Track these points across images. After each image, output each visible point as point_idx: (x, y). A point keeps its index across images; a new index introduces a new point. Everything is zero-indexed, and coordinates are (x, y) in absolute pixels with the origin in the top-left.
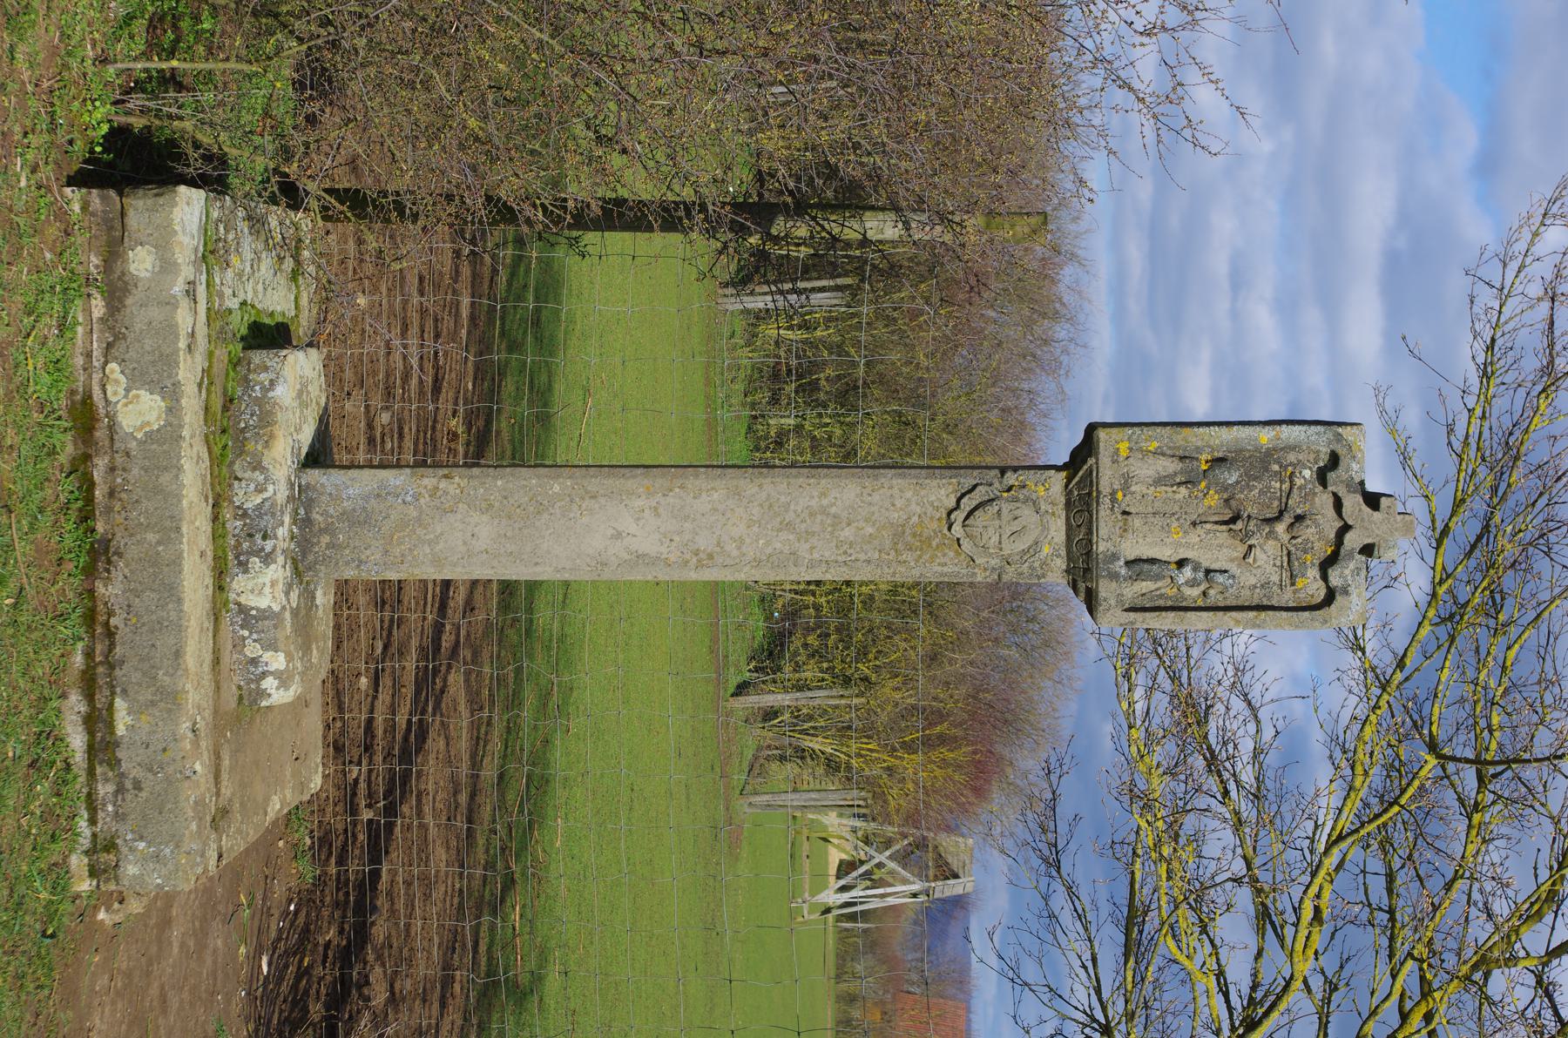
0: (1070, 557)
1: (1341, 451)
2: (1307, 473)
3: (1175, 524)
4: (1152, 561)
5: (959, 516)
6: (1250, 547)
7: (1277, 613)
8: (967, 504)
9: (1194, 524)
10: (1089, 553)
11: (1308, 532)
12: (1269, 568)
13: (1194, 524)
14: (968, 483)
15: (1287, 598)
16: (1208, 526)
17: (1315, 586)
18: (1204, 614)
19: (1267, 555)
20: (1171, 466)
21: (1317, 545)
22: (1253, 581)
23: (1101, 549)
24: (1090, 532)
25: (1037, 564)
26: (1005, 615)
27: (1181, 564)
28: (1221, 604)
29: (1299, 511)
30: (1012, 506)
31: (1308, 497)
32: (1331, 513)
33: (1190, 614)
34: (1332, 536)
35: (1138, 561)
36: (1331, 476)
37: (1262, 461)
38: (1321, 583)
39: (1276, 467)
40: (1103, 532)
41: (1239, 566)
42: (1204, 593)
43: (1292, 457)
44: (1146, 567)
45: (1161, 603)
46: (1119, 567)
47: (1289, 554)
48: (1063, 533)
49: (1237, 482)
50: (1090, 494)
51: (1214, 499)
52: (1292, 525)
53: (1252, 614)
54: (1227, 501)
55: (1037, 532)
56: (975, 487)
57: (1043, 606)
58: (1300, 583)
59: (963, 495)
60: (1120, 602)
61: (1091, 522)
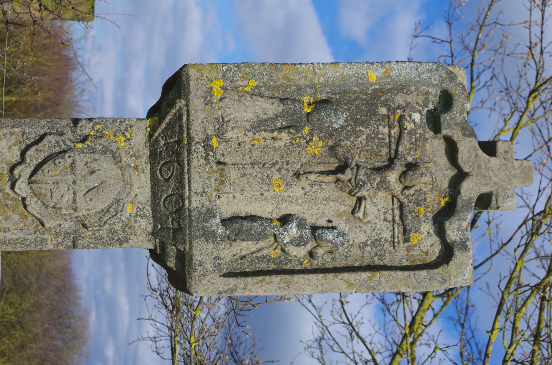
0: (156, 217)
1: (454, 91)
2: (417, 117)
3: (276, 176)
4: (253, 218)
5: (24, 171)
6: (360, 200)
7: (393, 274)
8: (34, 156)
9: (297, 175)
10: (180, 211)
11: (421, 182)
12: (380, 224)
13: (297, 175)
14: (35, 132)
15: (400, 256)
16: (313, 177)
17: (429, 242)
18: (313, 277)
19: (378, 207)
20: (272, 108)
21: (430, 197)
22: (362, 238)
23: (194, 204)
24: (181, 185)
25: (118, 227)
26: (56, 325)
27: (285, 220)
28: (329, 265)
29: (410, 159)
30: (88, 157)
31: (417, 144)
32: (443, 160)
33: (296, 277)
34: (446, 185)
35: (235, 218)
36: (445, 118)
37: (369, 104)
38: (435, 239)
39: (383, 111)
40: (197, 185)
41: (347, 221)
42: (311, 254)
43: (400, 99)
44: (246, 224)
45: (263, 266)
46: (215, 225)
47: (401, 207)
48: (148, 189)
49: (343, 128)
50: (179, 142)
51: (317, 147)
52: (404, 174)
53: (365, 275)
54: (332, 149)
55: (118, 188)
56: (42, 137)
57: (73, 321)
58: (414, 238)
59: (28, 147)
60: (218, 266)
61: (182, 174)
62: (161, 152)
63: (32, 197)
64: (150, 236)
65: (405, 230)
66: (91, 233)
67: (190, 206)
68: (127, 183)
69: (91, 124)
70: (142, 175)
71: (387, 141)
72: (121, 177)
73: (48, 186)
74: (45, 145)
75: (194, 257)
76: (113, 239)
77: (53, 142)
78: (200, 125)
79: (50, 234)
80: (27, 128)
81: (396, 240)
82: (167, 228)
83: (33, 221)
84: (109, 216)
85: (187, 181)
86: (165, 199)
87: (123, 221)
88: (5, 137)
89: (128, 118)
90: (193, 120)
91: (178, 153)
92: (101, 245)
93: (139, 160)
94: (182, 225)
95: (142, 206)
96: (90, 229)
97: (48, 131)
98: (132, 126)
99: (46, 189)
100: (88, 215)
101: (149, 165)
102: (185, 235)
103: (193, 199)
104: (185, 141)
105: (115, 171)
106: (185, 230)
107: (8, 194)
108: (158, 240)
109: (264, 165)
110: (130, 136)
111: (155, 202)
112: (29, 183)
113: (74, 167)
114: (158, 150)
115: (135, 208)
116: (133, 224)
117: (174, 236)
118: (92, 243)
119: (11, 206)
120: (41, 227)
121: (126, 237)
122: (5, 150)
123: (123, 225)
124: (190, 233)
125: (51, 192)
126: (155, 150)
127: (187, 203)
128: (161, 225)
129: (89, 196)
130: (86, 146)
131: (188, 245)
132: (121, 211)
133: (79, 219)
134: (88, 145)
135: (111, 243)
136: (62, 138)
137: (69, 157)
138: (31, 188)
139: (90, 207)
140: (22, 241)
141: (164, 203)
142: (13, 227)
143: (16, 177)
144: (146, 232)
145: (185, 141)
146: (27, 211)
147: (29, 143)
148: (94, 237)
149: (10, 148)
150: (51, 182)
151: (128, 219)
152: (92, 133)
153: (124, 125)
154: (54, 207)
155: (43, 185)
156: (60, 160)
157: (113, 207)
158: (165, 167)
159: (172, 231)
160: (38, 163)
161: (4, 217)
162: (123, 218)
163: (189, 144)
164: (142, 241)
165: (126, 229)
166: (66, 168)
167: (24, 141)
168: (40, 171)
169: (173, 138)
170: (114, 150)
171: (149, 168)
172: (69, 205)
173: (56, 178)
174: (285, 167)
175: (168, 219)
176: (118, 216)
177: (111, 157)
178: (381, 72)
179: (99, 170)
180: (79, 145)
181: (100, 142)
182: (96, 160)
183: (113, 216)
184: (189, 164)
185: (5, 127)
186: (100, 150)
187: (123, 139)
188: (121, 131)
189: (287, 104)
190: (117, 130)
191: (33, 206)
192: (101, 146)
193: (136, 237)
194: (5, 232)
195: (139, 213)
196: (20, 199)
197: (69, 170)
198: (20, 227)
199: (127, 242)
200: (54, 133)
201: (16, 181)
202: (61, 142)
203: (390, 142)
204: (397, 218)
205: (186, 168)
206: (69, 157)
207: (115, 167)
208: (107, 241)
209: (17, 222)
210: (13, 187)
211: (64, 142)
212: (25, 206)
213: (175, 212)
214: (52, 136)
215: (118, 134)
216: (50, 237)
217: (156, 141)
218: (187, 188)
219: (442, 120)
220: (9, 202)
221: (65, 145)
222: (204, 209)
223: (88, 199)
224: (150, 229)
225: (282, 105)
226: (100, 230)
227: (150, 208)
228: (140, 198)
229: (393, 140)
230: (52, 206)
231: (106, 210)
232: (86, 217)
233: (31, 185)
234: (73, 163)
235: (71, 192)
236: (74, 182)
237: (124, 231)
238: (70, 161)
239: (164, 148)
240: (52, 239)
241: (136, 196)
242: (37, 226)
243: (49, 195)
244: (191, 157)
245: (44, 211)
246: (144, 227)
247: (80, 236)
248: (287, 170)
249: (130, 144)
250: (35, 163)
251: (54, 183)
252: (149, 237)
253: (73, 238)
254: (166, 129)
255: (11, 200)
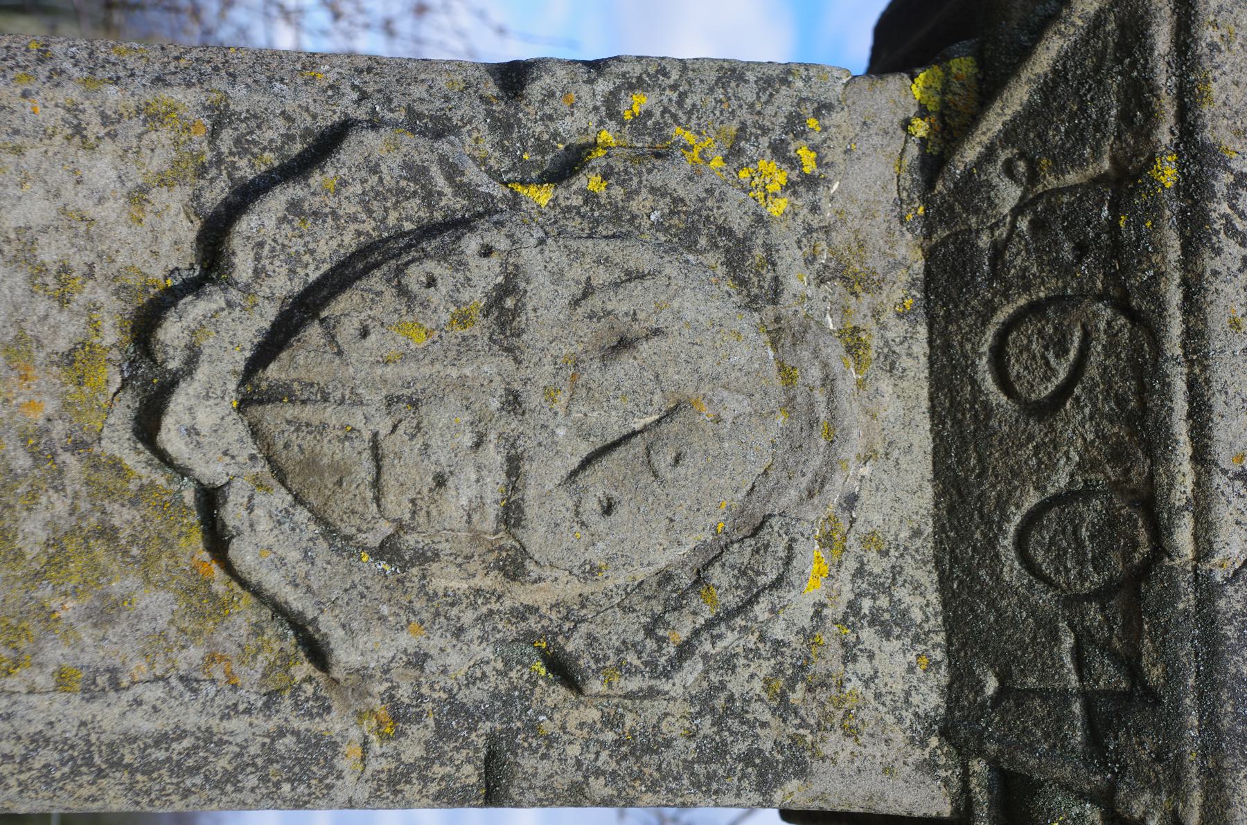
8: (278, 247)
24: (1142, 430)
25: (747, 681)
50: (1128, 180)
59: (246, 196)
61: (1145, 369)
62: (998, 250)
63: (258, 483)
64: (934, 741)
66: (593, 715)
67: (1204, 551)
68: (811, 423)
69: (603, 86)
70: (885, 385)
72: (778, 383)
73: (357, 421)
74: (343, 183)
76: (721, 751)
77: (391, 167)
79: (360, 714)
80: (239, 92)
82: (1044, 695)
83: (257, 630)
84: (707, 614)
85: (1180, 405)
86: (1033, 519)
87: (778, 645)
88: (113, 136)
89: (807, 67)
90: (1213, 47)
91: (1117, 247)
92: (653, 788)
93: (866, 298)
94: (1155, 674)
95: (886, 563)
96: (596, 686)
97: (361, 113)
98: (829, 107)
99: (349, 434)
100: (584, 601)
101: (923, 331)
102: (1172, 730)
103: (1225, 513)
104: (1168, 174)
105: (747, 348)
106: (1177, 702)
107: (116, 466)
108: (978, 766)
110: (819, 161)
111: (964, 536)
112: (244, 404)
113: (516, 312)
114: (984, 241)
115: (845, 575)
116: (837, 666)
117: (1095, 739)
118: (599, 773)
119: (133, 540)
120: (303, 668)
121: (794, 739)
122: (111, 211)
123: (778, 670)
124: (1210, 721)
125: (377, 457)
126: (964, 242)
127: (1183, 538)
128: (1003, 678)
129: (597, 483)
130: (577, 201)
131: (1196, 798)
132: (777, 584)
133: (533, 623)
134: (590, 197)
135: (711, 777)
136: (443, 146)
137: (487, 252)
138: (255, 432)
139: (596, 555)
140: (189, 752)
141: (1021, 542)
142: (139, 668)
143: (173, 365)
144: (908, 716)
145: (1168, 174)
146: (228, 567)
147: (249, 174)
148: (610, 736)
149: (139, 196)
150: (375, 398)
151: (808, 636)
152: (606, 136)
153: (784, 101)
154: (387, 550)
155: (330, 415)
156: (430, 266)
157: (728, 558)
158: (1029, 337)
159: (1077, 708)
160: (298, 287)
161: (87, 600)
162: (778, 631)
163: (1194, 190)
164: (888, 770)
165: (796, 697)
166: (463, 319)
167: (219, 161)
168: (314, 332)
169: (1081, 163)
170: (739, 224)
171: (921, 347)
172: (476, 537)
173: (409, 371)
175: (1055, 637)
176: (761, 610)
177: (721, 271)
179: (657, 332)
180: (542, 196)
181: (657, 179)
182: (642, 277)
183: (729, 615)
185: (116, 81)
186: (658, 226)
187: (781, 178)
188: (765, 131)
190: (743, 128)
191: (268, 539)
192: (664, 204)
193: (850, 744)
194: (90, 692)
195: (866, 604)
196: (189, 496)
197: (480, 328)
198: (183, 668)
199: (802, 772)
200: (395, 125)
201: (168, 387)
202: (435, 170)
205: (1175, 328)
206: (487, 252)
207: (747, 322)
208: (688, 765)
209: (163, 635)
210: (147, 427)
211: (452, 171)
212: (218, 541)
213: (1101, 595)
214: (386, 133)
215: (750, 149)
216: (354, 733)
217: (972, 188)
218: (1184, 449)
220: (122, 516)
221: (461, 189)
223: (591, 505)
224: (930, 700)
226: (652, 693)
227: (928, 578)
228: (871, 515)
230: (373, 540)
231: (686, 580)
232: (572, 615)
233: (256, 411)
234: (508, 288)
235: (494, 455)
236: (513, 402)
237: (784, 708)
238: (487, 274)
239: (1023, 225)
240: (365, 744)
241: (851, 501)
242: (286, 661)
243: (364, 470)
244: (1210, 263)
245: (328, 569)
246: (899, 688)
247: (533, 727)
249: (814, 208)
250: (283, 284)
251: (391, 401)
252: (924, 744)
253: (492, 738)
254: (1030, 114)
255: (134, 503)
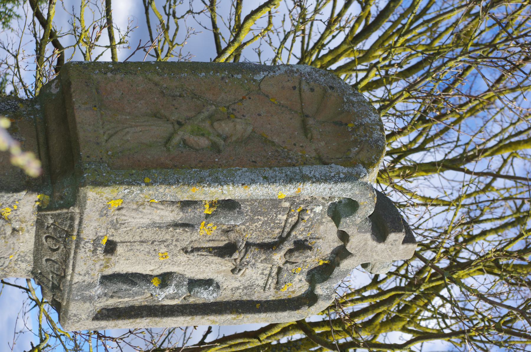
23: (76, 280)
40: (81, 267)
65: (277, 283)
71: (283, 224)
75: (69, 312)
78: (92, 230)
81: (268, 287)
98: (20, 200)
109: (152, 243)
124: (69, 296)
174: (174, 243)
178: (292, 192)
184: (75, 253)
189: (187, 212)
203: (285, 226)
204: (273, 274)
205: (72, 255)
219: (341, 223)
222: (86, 283)
225: (181, 213)
229: (288, 225)
248: (176, 245)
